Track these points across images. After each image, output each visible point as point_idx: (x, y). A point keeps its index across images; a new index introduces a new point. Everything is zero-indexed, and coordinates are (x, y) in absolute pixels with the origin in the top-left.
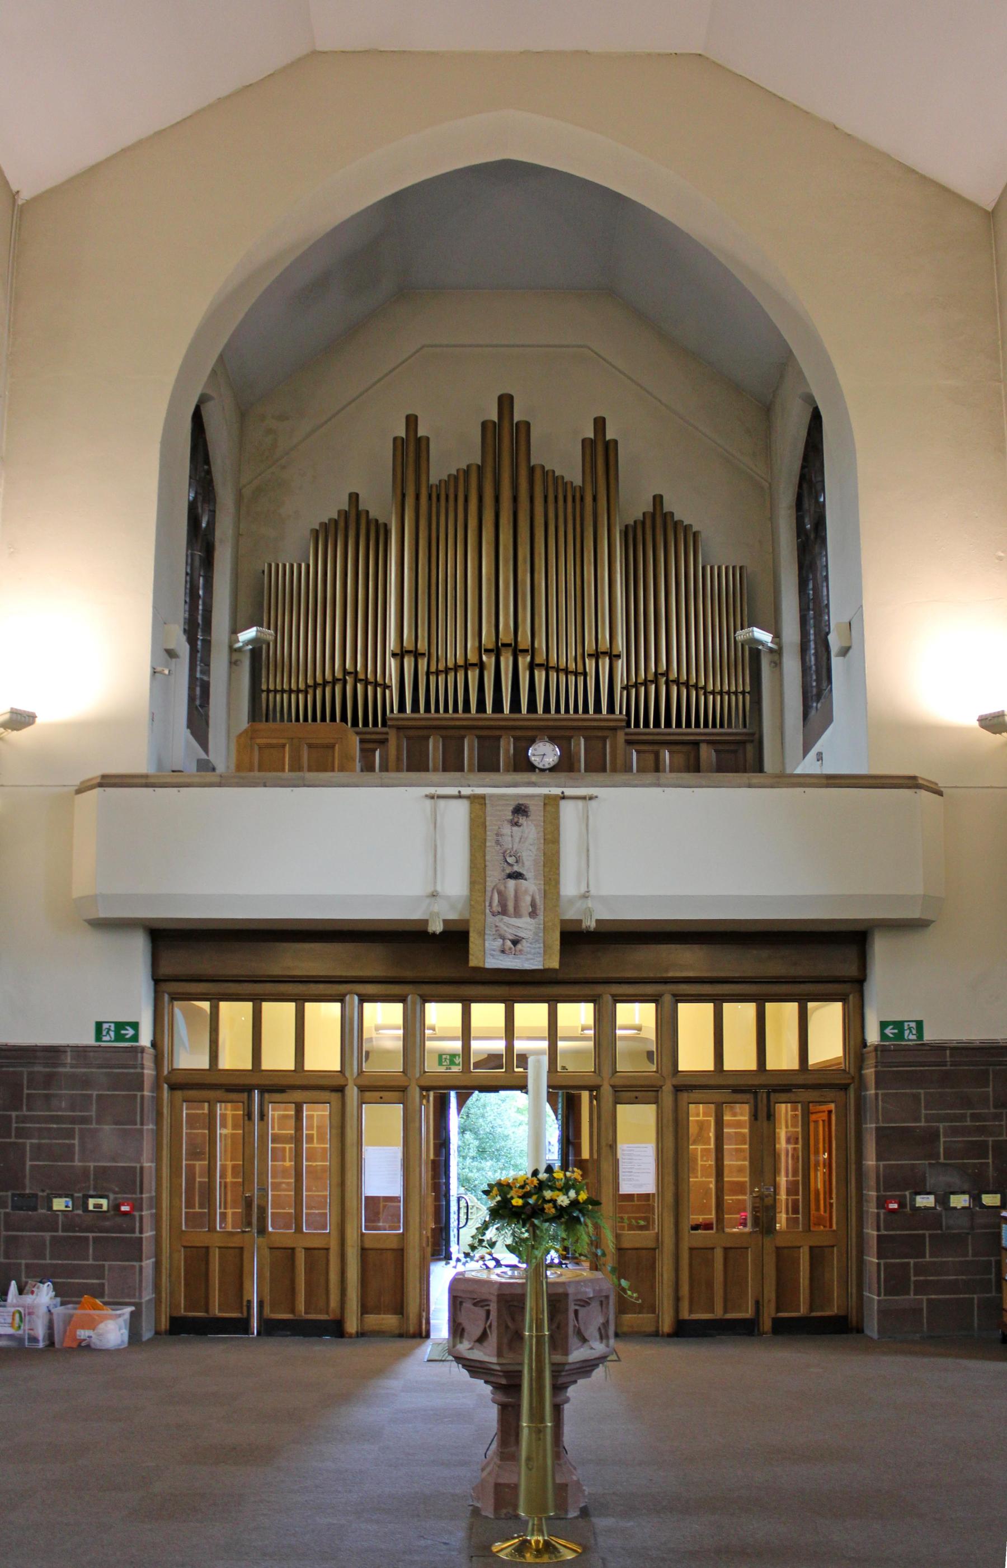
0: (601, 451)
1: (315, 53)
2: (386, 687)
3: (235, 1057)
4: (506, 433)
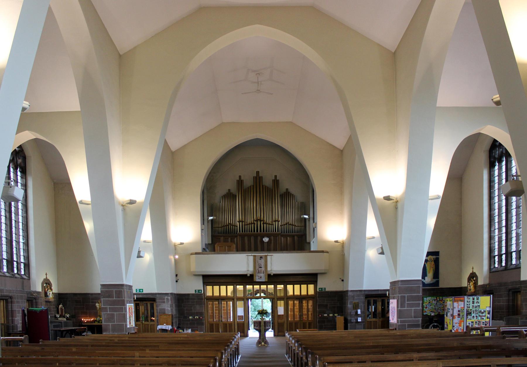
0: (276, 182)
1: (223, 123)
2: (236, 226)
3: (216, 294)
4: (258, 179)
